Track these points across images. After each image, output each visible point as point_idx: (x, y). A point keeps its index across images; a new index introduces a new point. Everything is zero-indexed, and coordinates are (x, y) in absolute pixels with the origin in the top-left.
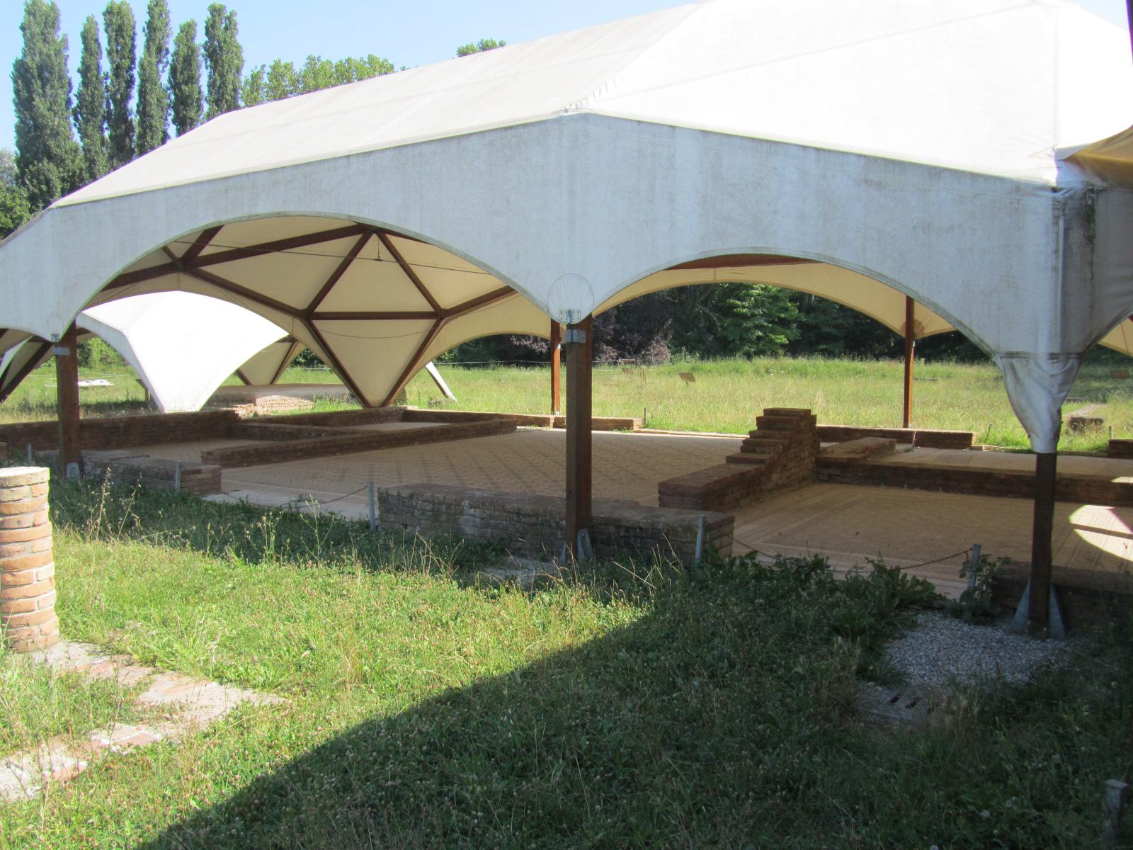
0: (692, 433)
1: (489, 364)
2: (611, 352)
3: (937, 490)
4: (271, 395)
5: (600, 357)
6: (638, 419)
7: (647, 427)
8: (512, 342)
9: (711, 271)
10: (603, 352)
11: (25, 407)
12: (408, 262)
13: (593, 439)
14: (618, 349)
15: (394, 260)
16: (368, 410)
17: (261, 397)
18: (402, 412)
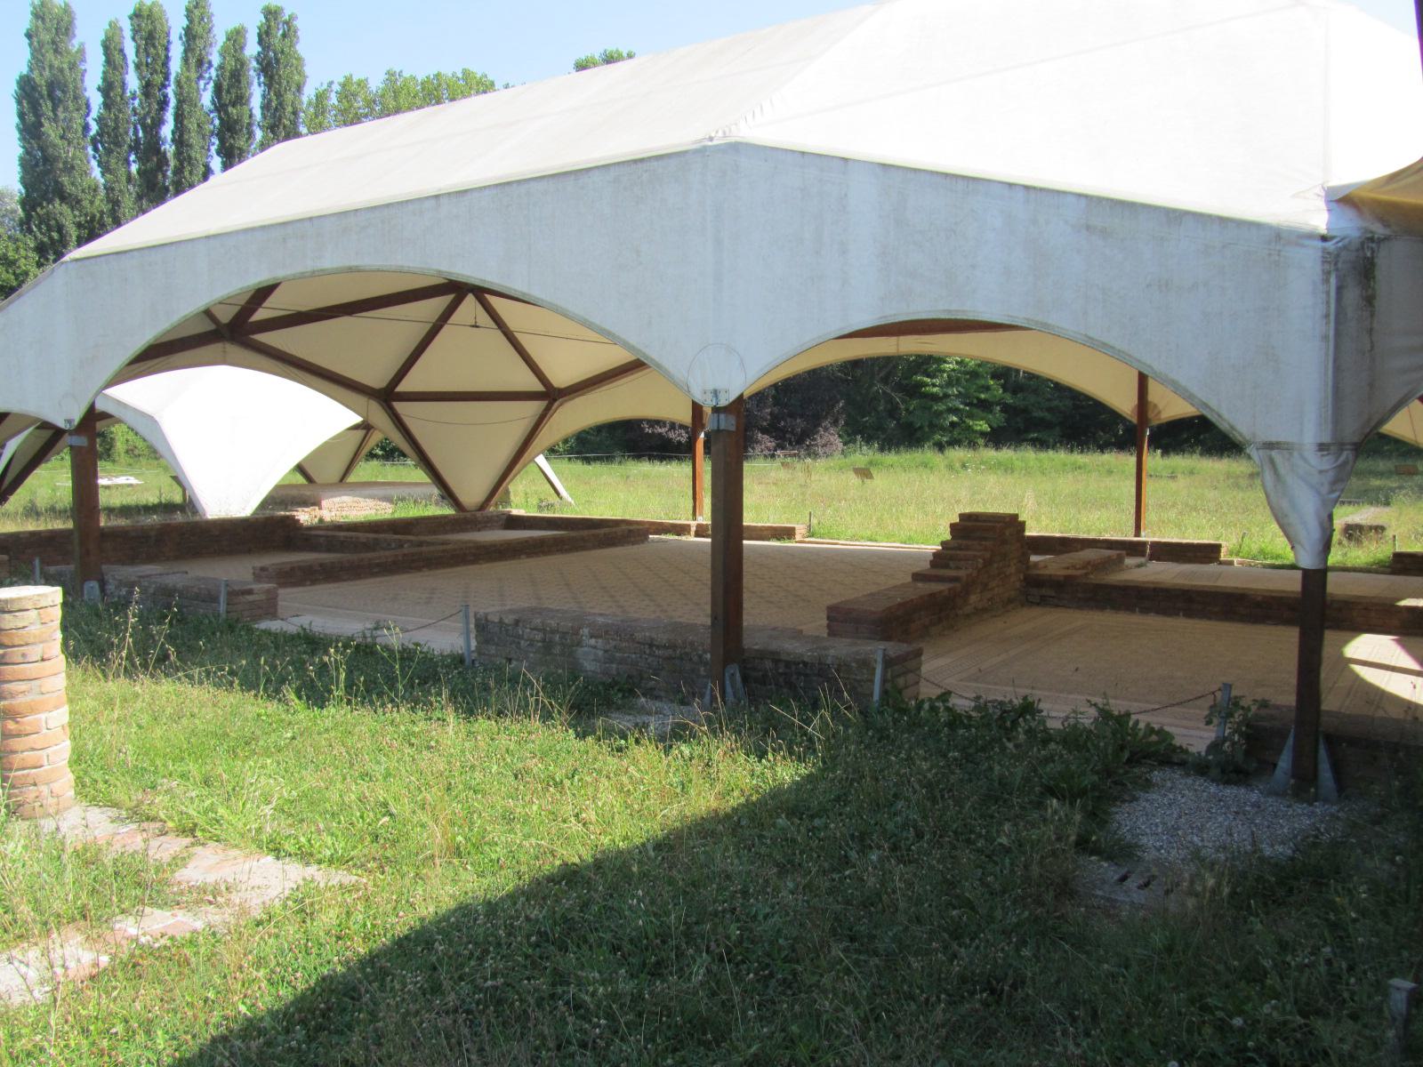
0: (869, 543)
1: (614, 457)
2: (767, 441)
3: (1177, 615)
4: (340, 496)
5: (753, 448)
6: (802, 526)
7: (812, 536)
8: (643, 429)
9: (893, 340)
10: (758, 442)
11: (32, 511)
12: (512, 329)
13: (745, 551)
14: (776, 438)
15: (494, 326)
16: (462, 515)
17: (328, 498)
18: (505, 517)
